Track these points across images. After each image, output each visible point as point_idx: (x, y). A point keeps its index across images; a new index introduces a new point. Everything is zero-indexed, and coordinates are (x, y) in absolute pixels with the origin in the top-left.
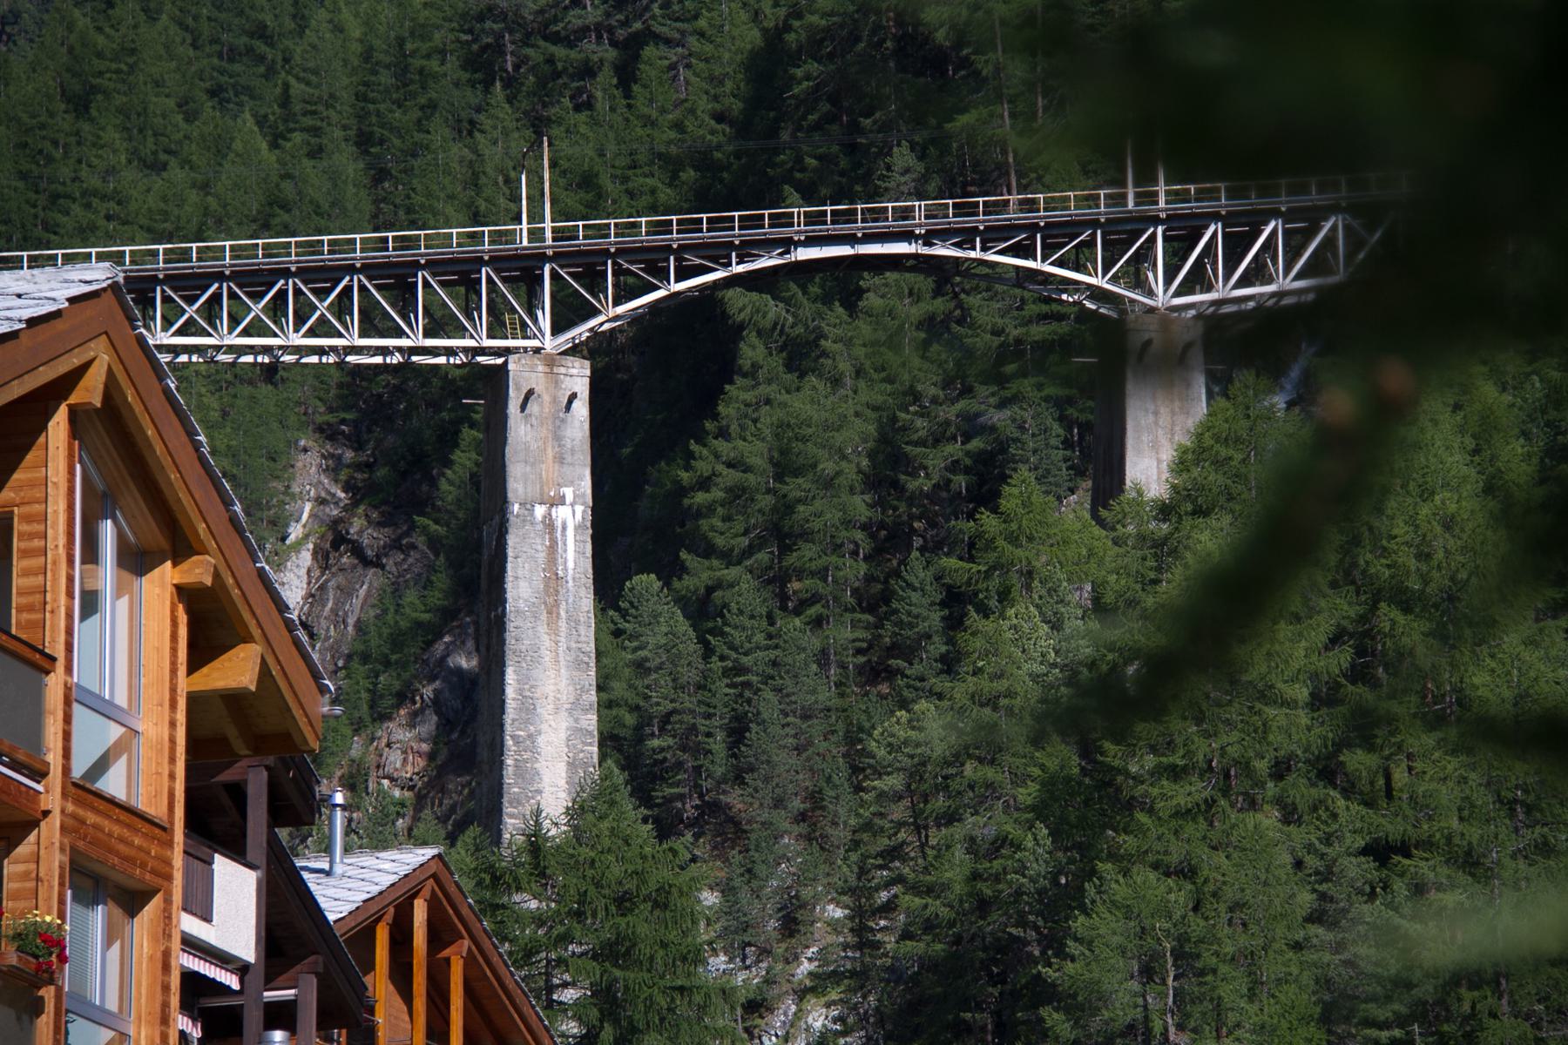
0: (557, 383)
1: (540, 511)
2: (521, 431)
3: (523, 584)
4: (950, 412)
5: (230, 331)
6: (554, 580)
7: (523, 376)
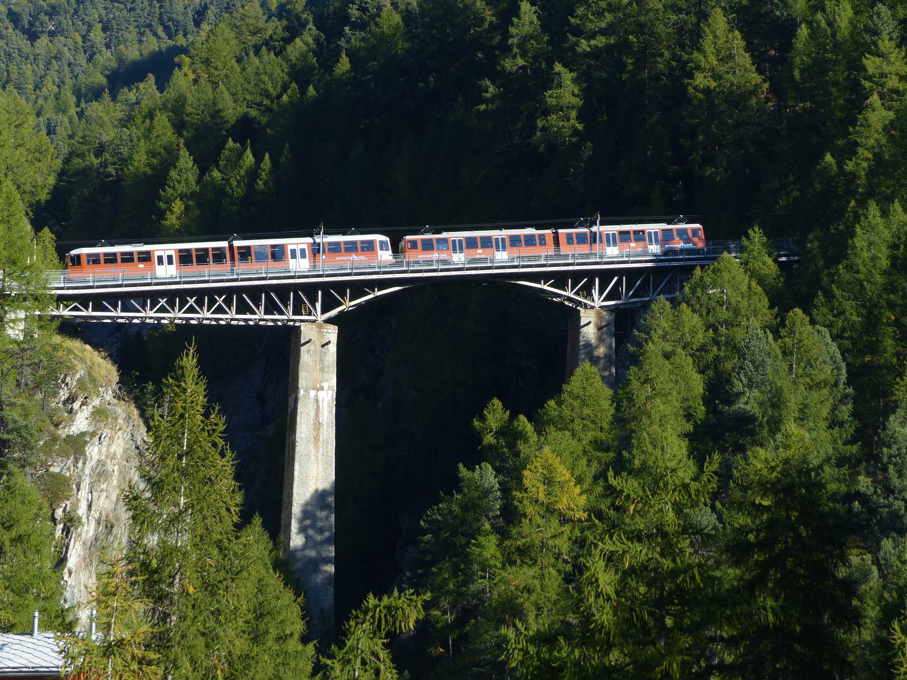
0: (323, 336)
1: (312, 393)
2: (307, 357)
3: (304, 426)
4: (244, 28)
5: (151, 310)
6: (317, 425)
7: (307, 332)
